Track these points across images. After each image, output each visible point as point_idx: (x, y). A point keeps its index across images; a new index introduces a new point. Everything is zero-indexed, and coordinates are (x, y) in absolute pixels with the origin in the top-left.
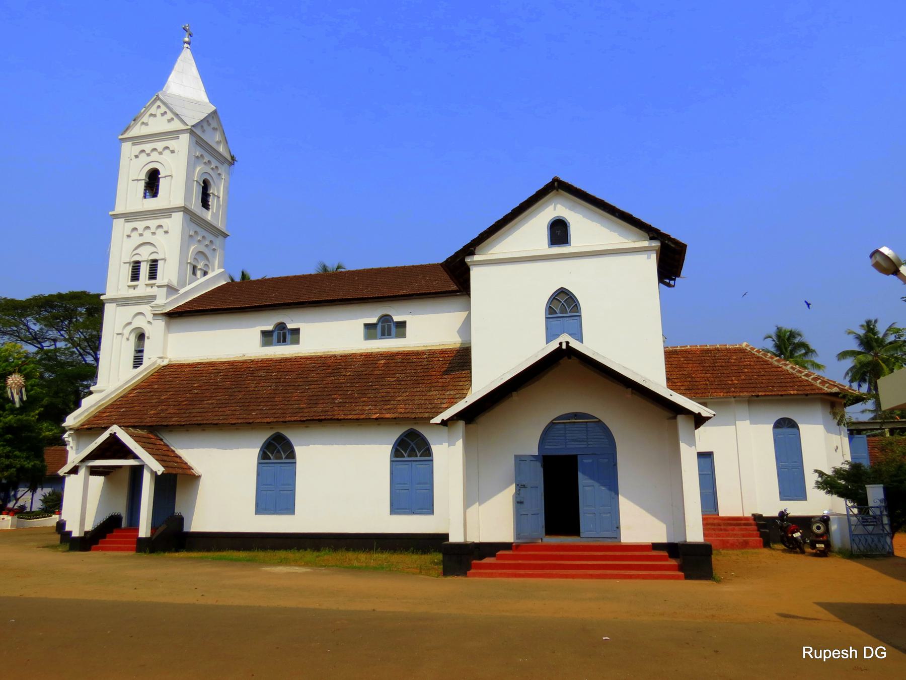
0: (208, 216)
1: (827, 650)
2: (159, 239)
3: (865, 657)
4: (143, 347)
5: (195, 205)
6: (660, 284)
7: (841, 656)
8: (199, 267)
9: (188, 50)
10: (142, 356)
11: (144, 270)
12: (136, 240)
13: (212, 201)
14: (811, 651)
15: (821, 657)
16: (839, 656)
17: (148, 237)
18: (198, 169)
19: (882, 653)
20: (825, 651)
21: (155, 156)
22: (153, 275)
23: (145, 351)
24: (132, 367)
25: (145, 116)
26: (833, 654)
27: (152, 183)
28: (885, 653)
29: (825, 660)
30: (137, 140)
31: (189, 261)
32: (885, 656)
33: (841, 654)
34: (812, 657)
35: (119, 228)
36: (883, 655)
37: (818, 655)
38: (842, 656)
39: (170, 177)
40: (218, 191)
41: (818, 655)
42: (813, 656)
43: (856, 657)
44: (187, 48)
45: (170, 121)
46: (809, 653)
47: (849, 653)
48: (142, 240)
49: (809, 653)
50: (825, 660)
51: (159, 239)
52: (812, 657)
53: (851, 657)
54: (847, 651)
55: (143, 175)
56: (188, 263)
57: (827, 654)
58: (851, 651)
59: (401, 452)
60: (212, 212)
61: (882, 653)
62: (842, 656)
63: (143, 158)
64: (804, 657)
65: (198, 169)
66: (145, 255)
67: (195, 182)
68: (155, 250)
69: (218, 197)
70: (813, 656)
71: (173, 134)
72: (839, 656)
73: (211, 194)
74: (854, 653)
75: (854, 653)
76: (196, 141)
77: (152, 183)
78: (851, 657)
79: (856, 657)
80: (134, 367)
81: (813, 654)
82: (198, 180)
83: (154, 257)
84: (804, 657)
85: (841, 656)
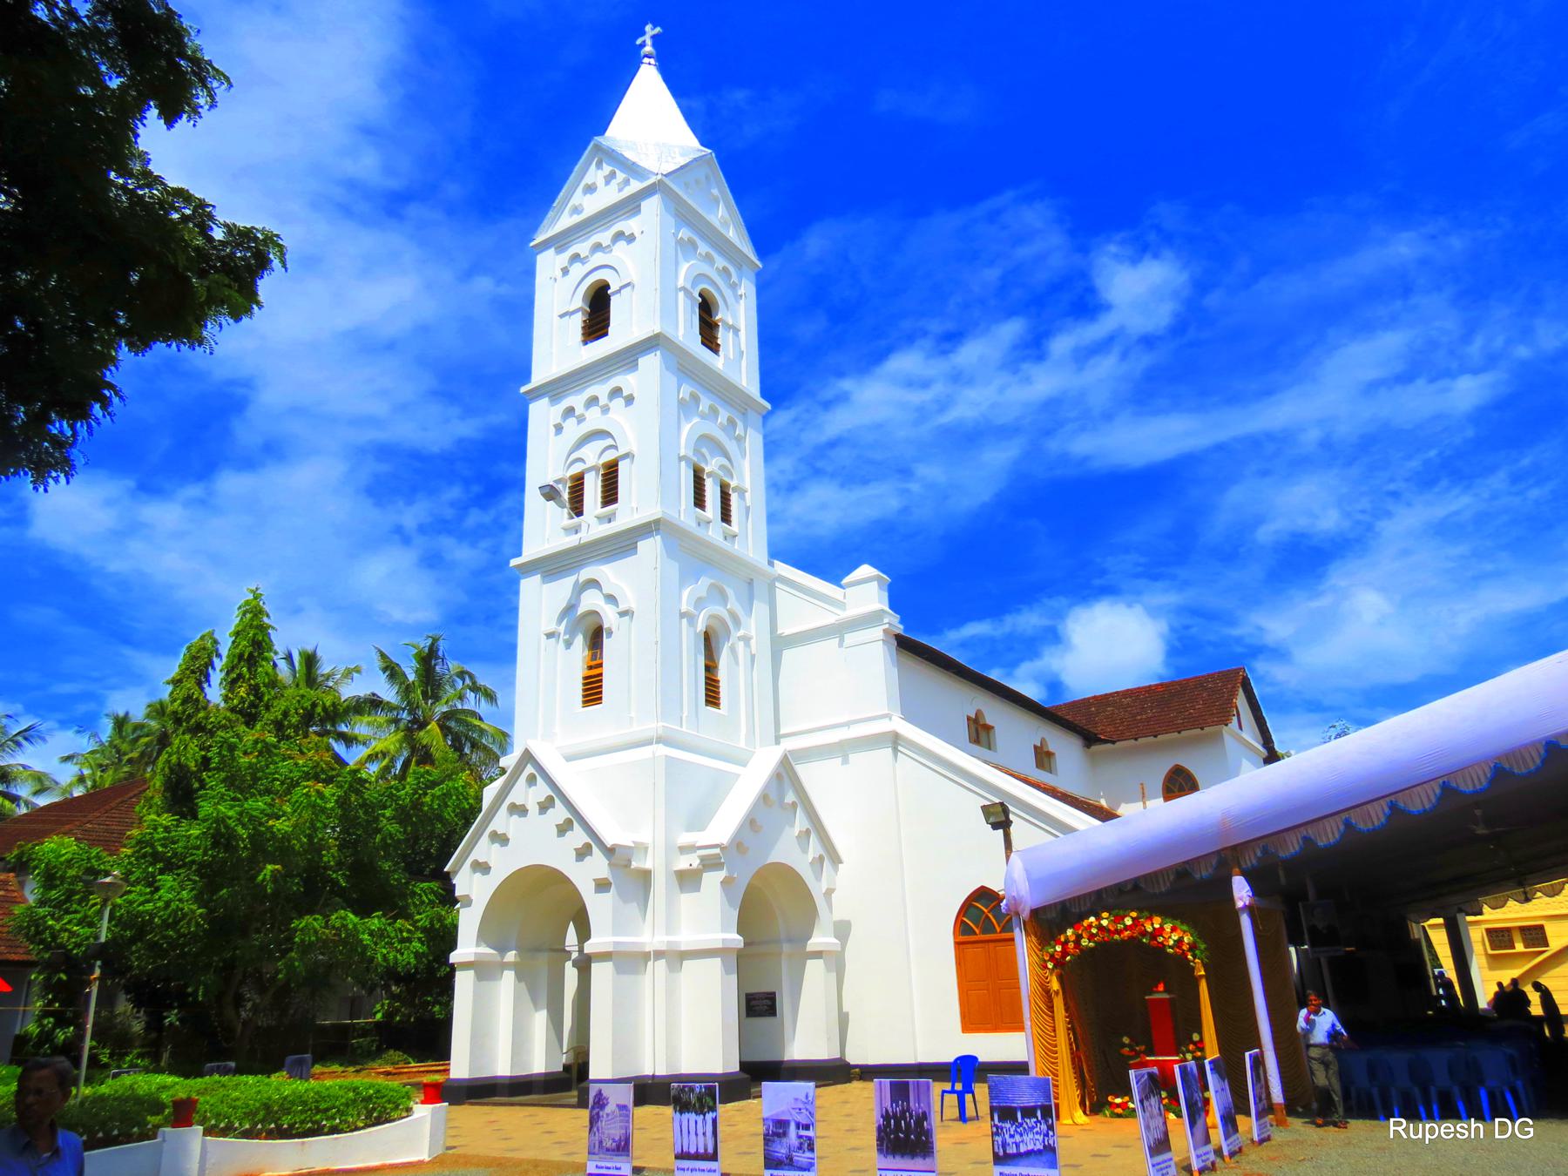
0: (718, 362)
1: (1431, 1125)
2: (618, 419)
3: (1497, 1136)
4: (601, 658)
5: (686, 331)
6: (572, 1051)
7: (1455, 1135)
8: (707, 469)
9: (652, 67)
10: (601, 675)
11: (593, 489)
12: (573, 430)
13: (722, 336)
14: (1404, 1127)
15: (1420, 1136)
16: (1452, 1135)
17: (594, 419)
18: (686, 429)
19: (1526, 1129)
20: (1428, 1126)
21: (599, 259)
22: (610, 494)
23: (604, 681)
24: (581, 705)
25: (577, 191)
26: (1442, 1131)
27: (597, 316)
28: (1531, 1130)
29: (1427, 1142)
30: (560, 242)
31: (682, 453)
32: (1531, 1135)
33: (1456, 1131)
34: (1405, 1137)
35: (541, 415)
36: (1529, 1133)
37: (1416, 1133)
38: (1458, 1135)
39: (629, 288)
40: (735, 317)
41: (1416, 1133)
42: (1408, 1134)
43: (1482, 1137)
44: (649, 64)
45: (627, 182)
46: (1400, 1129)
47: (1469, 1130)
48: (586, 428)
49: (1400, 1129)
50: (1427, 1142)
51: (618, 419)
52: (1405, 1137)
53: (1473, 1137)
54: (1466, 1126)
55: (579, 302)
56: (681, 459)
57: (1432, 1131)
58: (1473, 1126)
59: (978, 907)
60: (726, 357)
61: (1526, 1129)
62: (1458, 1135)
63: (578, 270)
64: (1392, 1137)
65: (686, 429)
66: (593, 455)
67: (681, 295)
68: (612, 443)
69: (736, 331)
70: (1408, 1134)
71: (630, 206)
72: (1452, 1135)
73: (720, 324)
74: (1477, 1129)
75: (1477, 1129)
76: (678, 363)
77: (597, 316)
78: (1473, 1137)
79: (1482, 1137)
80: (584, 702)
81: (1406, 1130)
82: (688, 286)
83: (609, 456)
84: (1392, 1137)
85: (1455, 1135)
